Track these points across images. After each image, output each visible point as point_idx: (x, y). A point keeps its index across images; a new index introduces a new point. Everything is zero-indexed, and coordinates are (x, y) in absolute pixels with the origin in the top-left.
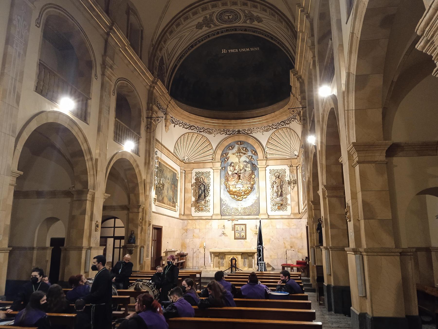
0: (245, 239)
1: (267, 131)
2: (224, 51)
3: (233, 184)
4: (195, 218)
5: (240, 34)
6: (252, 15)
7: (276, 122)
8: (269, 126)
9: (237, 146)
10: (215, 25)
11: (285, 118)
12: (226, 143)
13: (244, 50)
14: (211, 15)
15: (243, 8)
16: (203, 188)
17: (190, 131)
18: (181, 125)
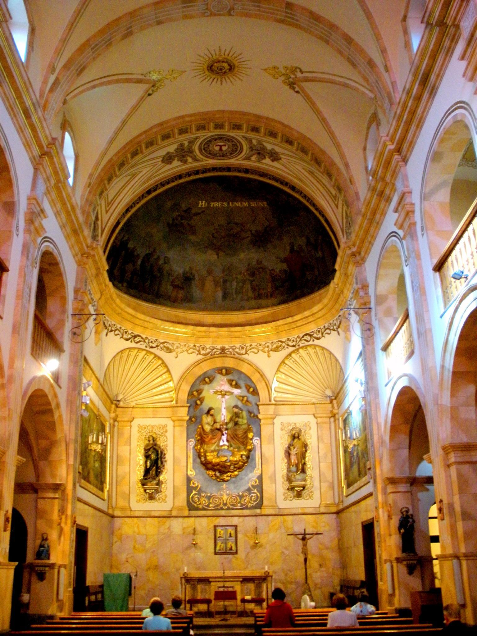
0: (236, 553)
1: (277, 349)
2: (202, 204)
3: (213, 448)
4: (137, 514)
6: (264, 148)
7: (294, 335)
10: (196, 160)
11: (312, 328)
12: (199, 371)
13: (238, 204)
14: (191, 142)
15: (251, 135)
16: (153, 457)
17: (133, 345)
18: (117, 332)
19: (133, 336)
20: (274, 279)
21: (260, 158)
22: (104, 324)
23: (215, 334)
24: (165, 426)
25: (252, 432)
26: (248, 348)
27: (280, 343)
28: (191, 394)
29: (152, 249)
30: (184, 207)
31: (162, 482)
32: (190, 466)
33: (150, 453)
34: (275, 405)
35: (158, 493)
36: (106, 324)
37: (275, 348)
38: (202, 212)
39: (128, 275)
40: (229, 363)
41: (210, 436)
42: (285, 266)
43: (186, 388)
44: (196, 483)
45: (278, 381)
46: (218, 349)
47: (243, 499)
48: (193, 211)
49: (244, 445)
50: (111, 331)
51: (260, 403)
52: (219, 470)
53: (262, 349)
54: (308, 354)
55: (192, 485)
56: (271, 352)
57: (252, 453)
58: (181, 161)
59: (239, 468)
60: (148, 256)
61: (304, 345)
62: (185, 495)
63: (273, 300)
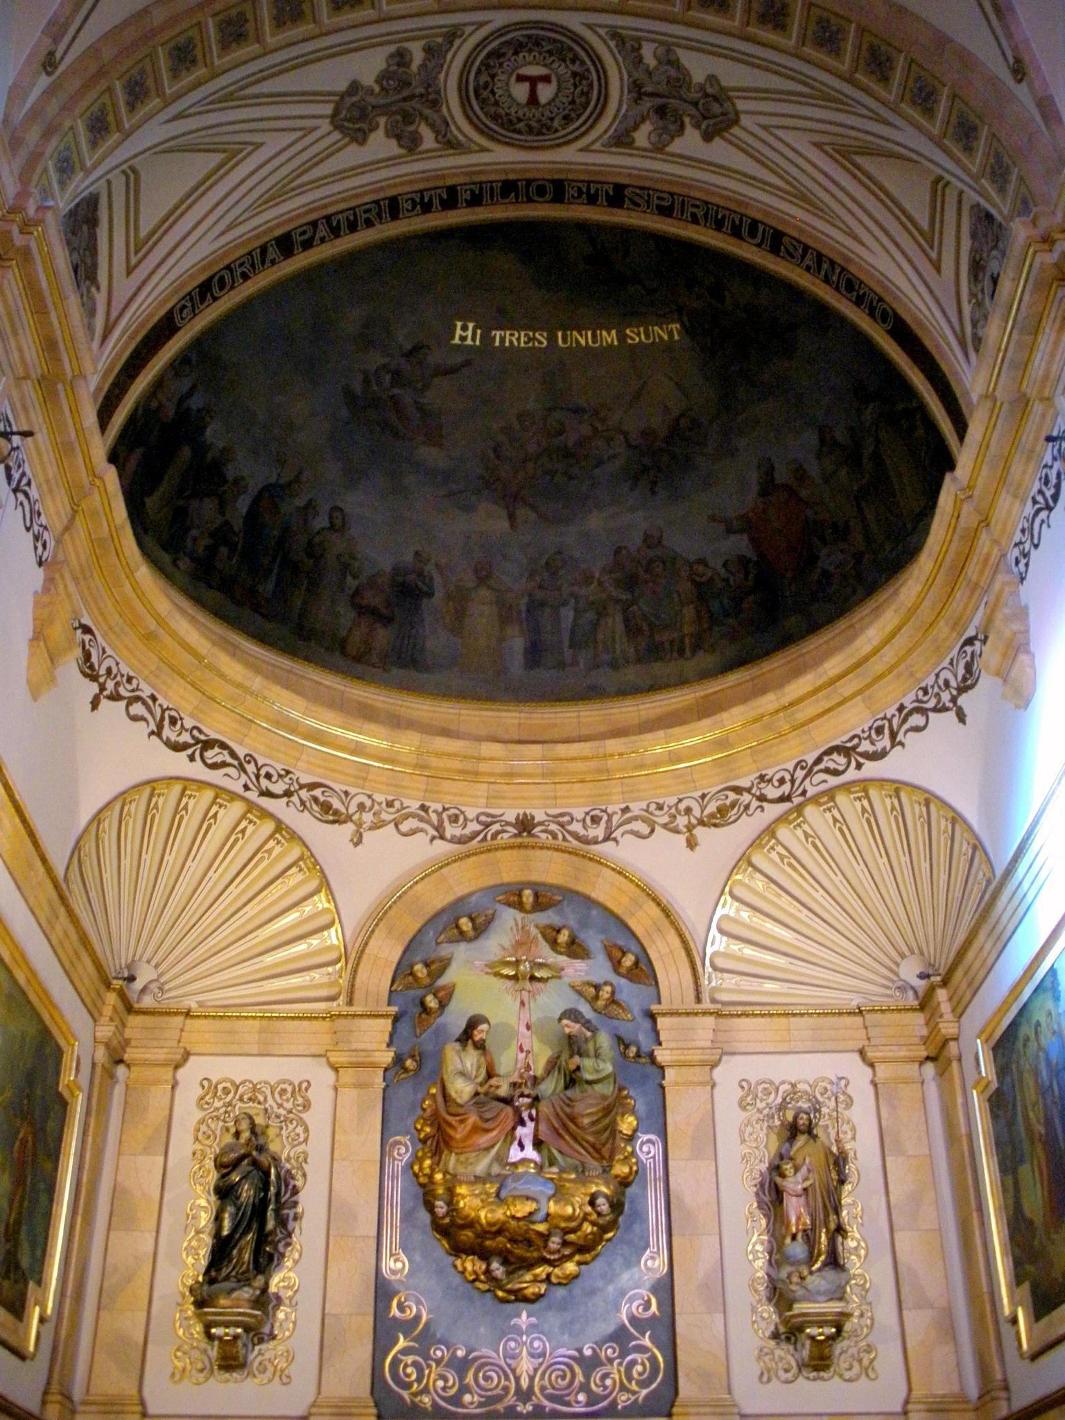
1: (720, 818)
2: (466, 334)
3: (480, 1167)
5: (582, 226)
6: (680, 80)
7: (783, 761)
8: (737, 790)
9: (509, 918)
11: (853, 721)
12: (436, 898)
13: (584, 339)
16: (247, 1193)
17: (197, 770)
18: (137, 709)
19: (198, 741)
20: (703, 591)
21: (665, 129)
22: (87, 656)
23: (499, 767)
24: (300, 1089)
25: (633, 1112)
26: (615, 819)
27: (732, 796)
28: (403, 971)
29: (288, 476)
30: (403, 337)
31: (278, 1298)
32: (391, 1236)
33: (235, 1177)
34: (718, 1014)
35: (261, 1341)
36: (94, 659)
37: (712, 816)
38: (468, 363)
39: (198, 540)
40: (549, 869)
41: (473, 1119)
42: (740, 544)
43: (386, 952)
44: (412, 1307)
45: (722, 931)
46: (508, 824)
47: (597, 1375)
48: (435, 357)
50: (115, 697)
52: (503, 1258)
53: (666, 819)
54: (841, 823)
55: (395, 1311)
56: (699, 831)
57: (630, 1191)
58: (398, 137)
59: (582, 1249)
60: (271, 494)
61: (823, 787)
62: (363, 1352)
63: (706, 660)
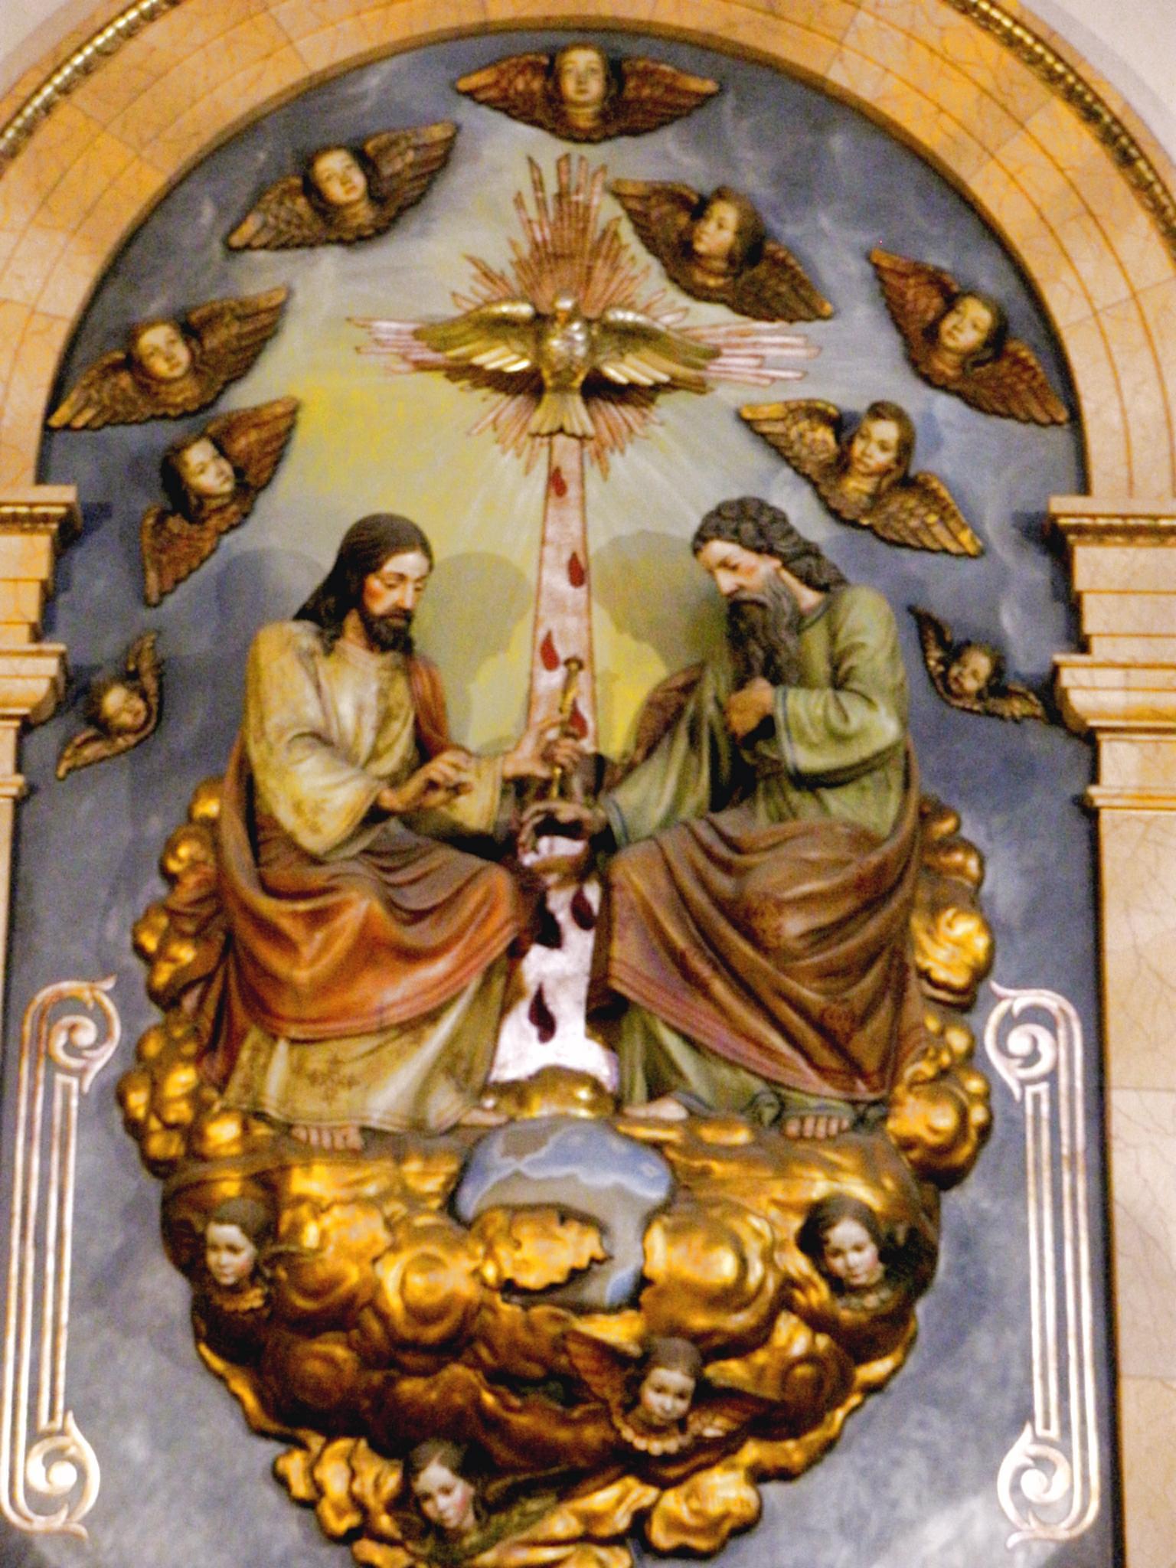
3: (386, 1100)
9: (507, 162)
25: (974, 901)
49: (855, 1069)
51: (1104, 501)
57: (957, 1202)
